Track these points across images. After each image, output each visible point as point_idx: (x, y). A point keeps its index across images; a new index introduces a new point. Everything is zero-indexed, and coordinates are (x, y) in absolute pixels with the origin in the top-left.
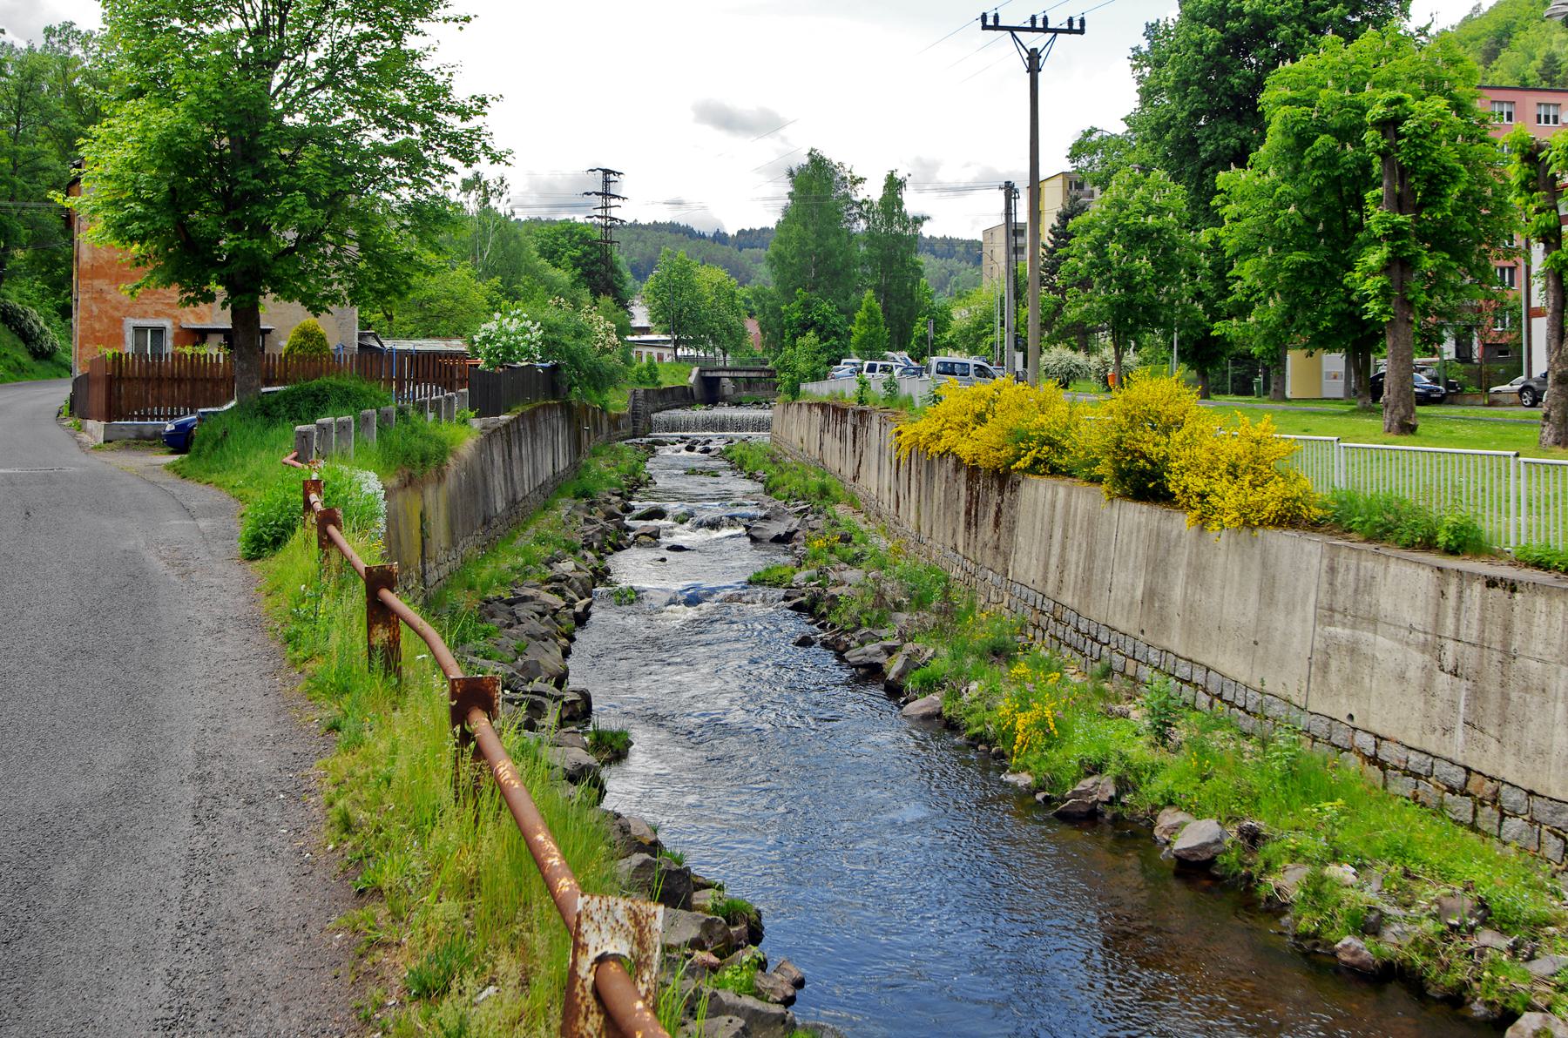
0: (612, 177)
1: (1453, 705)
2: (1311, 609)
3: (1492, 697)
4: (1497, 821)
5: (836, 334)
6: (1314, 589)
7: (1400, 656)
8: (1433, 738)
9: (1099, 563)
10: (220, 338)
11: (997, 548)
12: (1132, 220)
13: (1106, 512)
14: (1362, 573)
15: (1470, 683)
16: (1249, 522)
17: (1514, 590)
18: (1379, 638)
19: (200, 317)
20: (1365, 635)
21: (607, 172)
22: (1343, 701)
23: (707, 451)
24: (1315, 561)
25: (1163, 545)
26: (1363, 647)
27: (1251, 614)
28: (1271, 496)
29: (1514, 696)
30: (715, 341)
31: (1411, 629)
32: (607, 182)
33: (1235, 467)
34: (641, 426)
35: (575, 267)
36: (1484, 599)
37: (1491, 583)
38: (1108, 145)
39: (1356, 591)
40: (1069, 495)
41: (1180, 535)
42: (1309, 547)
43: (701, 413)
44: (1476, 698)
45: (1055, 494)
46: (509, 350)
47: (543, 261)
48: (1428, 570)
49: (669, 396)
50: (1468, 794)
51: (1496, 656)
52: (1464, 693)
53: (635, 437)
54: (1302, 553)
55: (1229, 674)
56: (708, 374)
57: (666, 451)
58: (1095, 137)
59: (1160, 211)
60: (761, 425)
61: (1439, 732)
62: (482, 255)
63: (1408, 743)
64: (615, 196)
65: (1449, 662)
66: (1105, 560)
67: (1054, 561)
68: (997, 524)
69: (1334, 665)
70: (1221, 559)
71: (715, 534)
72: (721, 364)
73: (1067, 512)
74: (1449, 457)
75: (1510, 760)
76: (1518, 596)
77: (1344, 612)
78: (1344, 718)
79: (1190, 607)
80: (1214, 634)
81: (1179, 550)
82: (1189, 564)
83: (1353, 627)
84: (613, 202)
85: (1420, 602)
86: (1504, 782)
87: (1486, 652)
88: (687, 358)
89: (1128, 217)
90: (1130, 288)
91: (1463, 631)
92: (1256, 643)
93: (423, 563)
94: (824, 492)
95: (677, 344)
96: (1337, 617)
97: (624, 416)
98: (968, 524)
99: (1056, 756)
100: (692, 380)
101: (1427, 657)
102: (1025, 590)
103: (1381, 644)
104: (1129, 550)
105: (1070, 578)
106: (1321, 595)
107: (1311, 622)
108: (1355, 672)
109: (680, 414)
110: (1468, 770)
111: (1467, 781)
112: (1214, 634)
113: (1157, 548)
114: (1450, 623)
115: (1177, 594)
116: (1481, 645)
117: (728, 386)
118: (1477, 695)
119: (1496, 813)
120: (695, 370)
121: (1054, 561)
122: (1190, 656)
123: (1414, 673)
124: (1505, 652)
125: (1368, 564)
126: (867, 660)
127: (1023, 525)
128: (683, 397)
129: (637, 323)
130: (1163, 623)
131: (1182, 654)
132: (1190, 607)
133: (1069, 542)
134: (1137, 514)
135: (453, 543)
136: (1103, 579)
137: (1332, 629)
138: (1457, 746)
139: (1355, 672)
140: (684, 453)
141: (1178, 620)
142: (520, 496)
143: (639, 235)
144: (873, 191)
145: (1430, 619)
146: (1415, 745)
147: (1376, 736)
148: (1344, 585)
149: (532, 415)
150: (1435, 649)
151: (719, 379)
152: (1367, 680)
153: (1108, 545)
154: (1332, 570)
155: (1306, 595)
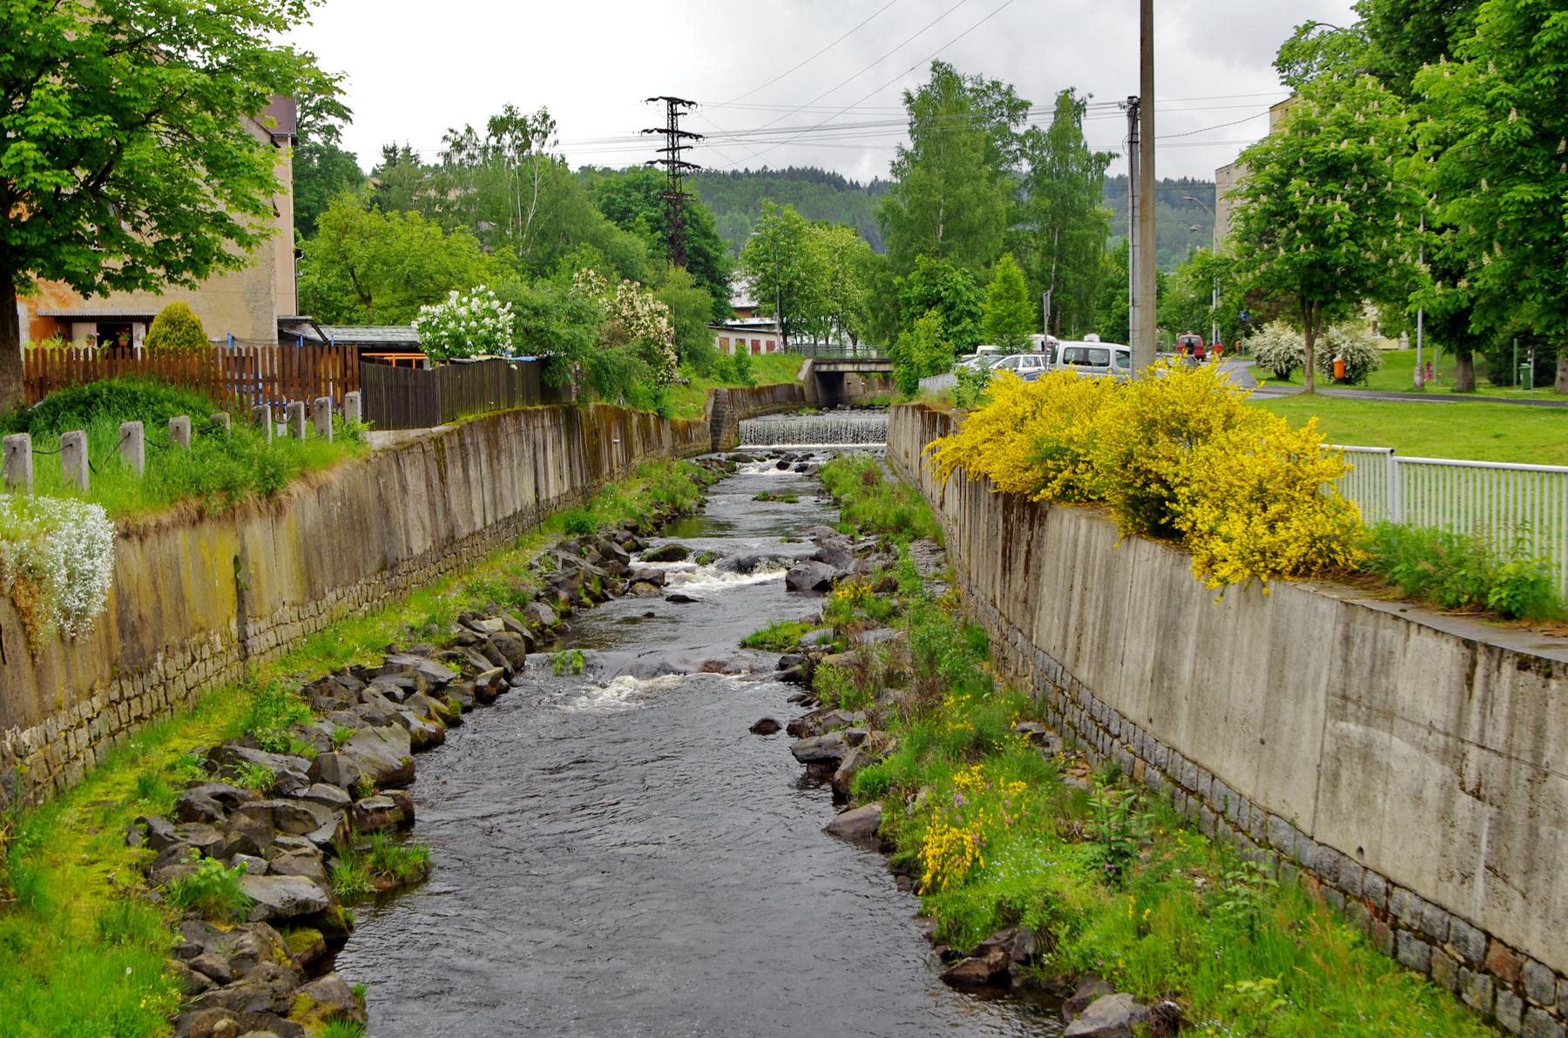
0: (680, 108)
1: (1474, 840)
2: (1321, 696)
3: (1518, 831)
4: (1518, 1013)
5: (971, 314)
6: (1326, 668)
7: (1416, 767)
8: (1450, 887)
9: (1114, 624)
10: (92, 329)
11: (1025, 601)
12: (1320, 148)
13: (1123, 555)
14: (1379, 646)
15: (1494, 809)
16: (1264, 566)
17: (1549, 676)
18: (1396, 740)
19: (63, 301)
20: (1381, 736)
21: (673, 101)
22: (1353, 828)
23: (801, 469)
24: (1329, 627)
25: (1175, 601)
26: (1377, 751)
27: (1259, 702)
28: (1293, 539)
29: (1544, 830)
30: (842, 324)
31: (1431, 728)
32: (673, 115)
33: (1261, 490)
34: (724, 437)
35: (653, 231)
36: (1514, 686)
37: (1524, 664)
38: (1338, 46)
39: (1372, 670)
40: (1090, 530)
41: (1191, 589)
42: (1323, 606)
43: (806, 420)
44: (1500, 832)
45: (1078, 528)
46: (458, 341)
47: (611, 224)
48: (1452, 643)
49: (768, 396)
50: (1487, 972)
51: (1526, 772)
52: (1487, 824)
53: (714, 450)
54: (1316, 610)
55: (1234, 784)
56: (824, 368)
57: (752, 470)
58: (1314, 34)
59: (1363, 135)
60: (881, 435)
61: (1458, 878)
62: (524, 216)
63: (1422, 892)
64: (685, 134)
65: (1471, 778)
66: (1120, 621)
67: (1073, 620)
68: (1027, 571)
69: (1345, 775)
70: (1230, 623)
71: (745, 580)
72: (849, 355)
73: (1088, 553)
74: (1511, 476)
75: (1537, 925)
76: (1554, 684)
77: (1357, 703)
78: (1352, 853)
79: (1199, 689)
80: (1221, 726)
81: (1190, 608)
82: (1199, 628)
83: (1368, 724)
84: (683, 141)
85: (1442, 690)
86: (1529, 957)
87: (1514, 764)
88: (798, 349)
89: (1315, 144)
90: (1322, 242)
91: (1488, 733)
92: (1262, 742)
93: (242, 623)
94: (902, 524)
95: (786, 330)
96: (1351, 707)
97: (698, 424)
98: (1004, 574)
99: (971, 894)
100: (802, 376)
101: (1448, 770)
102: (1048, 660)
103: (1397, 748)
104: (1142, 608)
105: (1086, 647)
106: (1334, 675)
107: (1321, 715)
108: (1367, 787)
109: (777, 422)
110: (1489, 937)
111: (1487, 950)
112: (1221, 726)
113: (1168, 607)
114: (1474, 719)
115: (1186, 670)
116: (1508, 755)
117: (854, 385)
118: (1500, 827)
119: (1518, 1002)
120: (808, 363)
121: (1073, 620)
122: (1195, 756)
123: (1432, 793)
124: (1536, 765)
125: (1390, 634)
126: (820, 753)
127: (1047, 569)
128: (791, 399)
129: (736, 303)
130: (1168, 715)
131: (1188, 754)
132: (1199, 689)
133: (1088, 595)
134: (1148, 555)
135: (312, 592)
136: (1116, 647)
137: (1343, 725)
138: (1475, 902)
139: (1367, 787)
140: (775, 472)
141: (1185, 706)
142: (464, 531)
143: (768, 186)
144: (1041, 119)
145: (1452, 716)
146: (1430, 896)
147: (1388, 881)
148: (1359, 664)
149: (495, 423)
150: (1454, 756)
151: (842, 373)
152: (1380, 800)
153: (1123, 599)
154: (1347, 640)
155: (1318, 674)
